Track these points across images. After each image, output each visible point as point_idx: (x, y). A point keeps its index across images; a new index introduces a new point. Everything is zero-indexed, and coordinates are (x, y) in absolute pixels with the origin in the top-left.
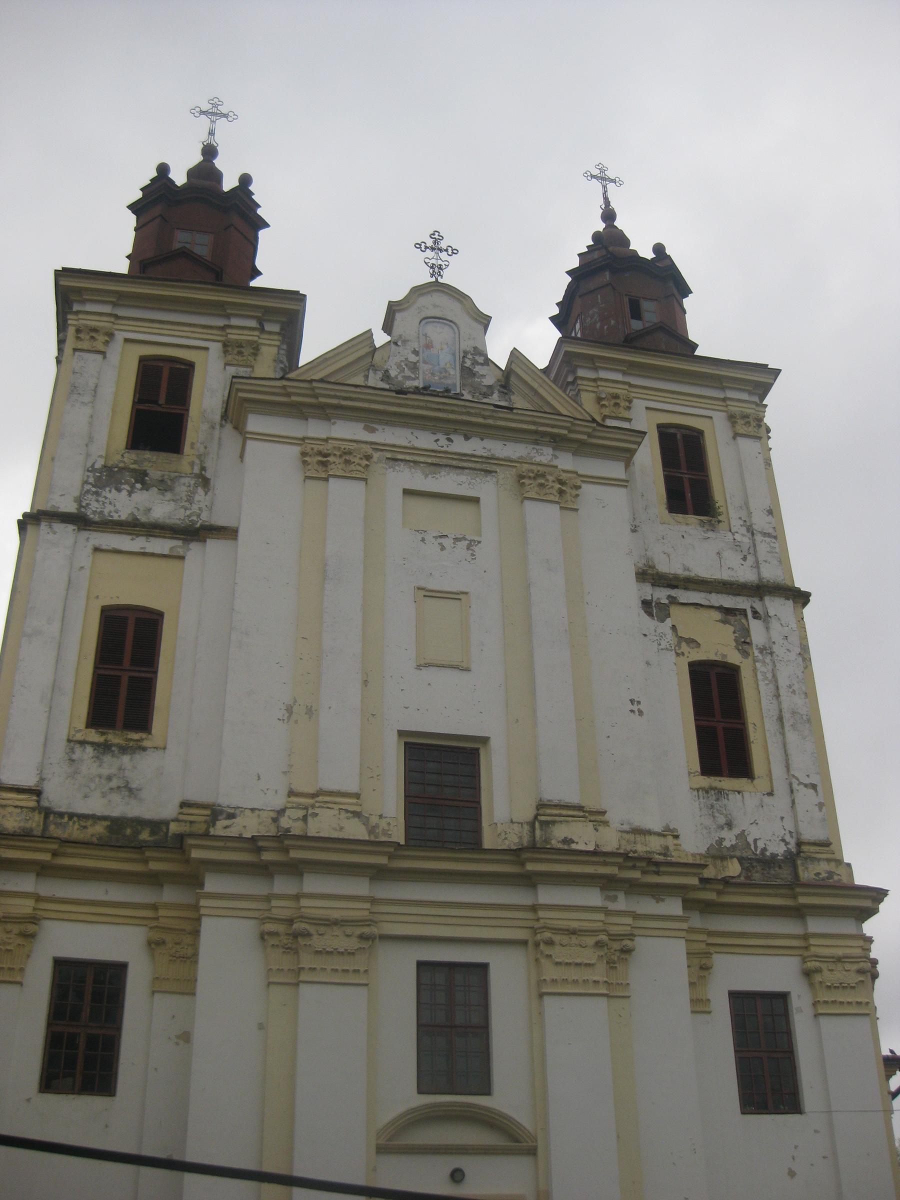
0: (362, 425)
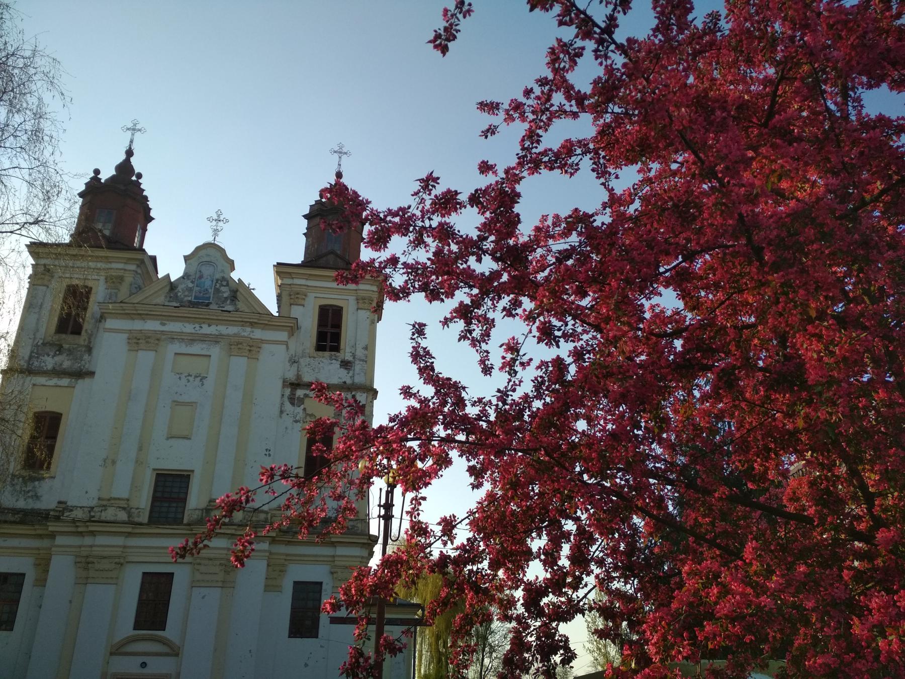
0: (159, 322)
